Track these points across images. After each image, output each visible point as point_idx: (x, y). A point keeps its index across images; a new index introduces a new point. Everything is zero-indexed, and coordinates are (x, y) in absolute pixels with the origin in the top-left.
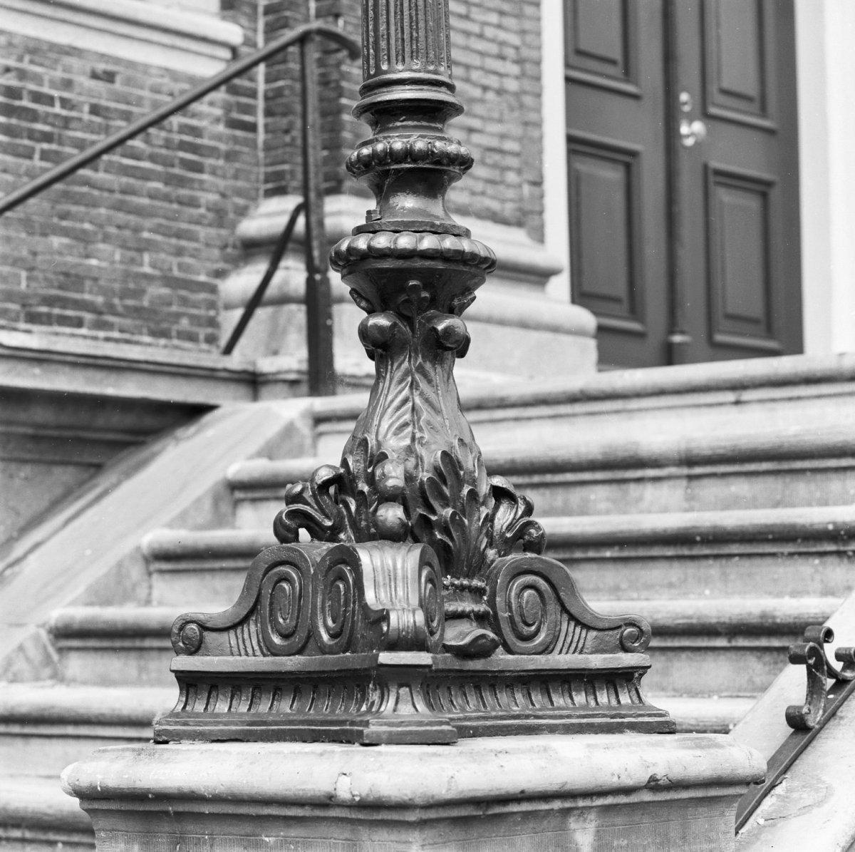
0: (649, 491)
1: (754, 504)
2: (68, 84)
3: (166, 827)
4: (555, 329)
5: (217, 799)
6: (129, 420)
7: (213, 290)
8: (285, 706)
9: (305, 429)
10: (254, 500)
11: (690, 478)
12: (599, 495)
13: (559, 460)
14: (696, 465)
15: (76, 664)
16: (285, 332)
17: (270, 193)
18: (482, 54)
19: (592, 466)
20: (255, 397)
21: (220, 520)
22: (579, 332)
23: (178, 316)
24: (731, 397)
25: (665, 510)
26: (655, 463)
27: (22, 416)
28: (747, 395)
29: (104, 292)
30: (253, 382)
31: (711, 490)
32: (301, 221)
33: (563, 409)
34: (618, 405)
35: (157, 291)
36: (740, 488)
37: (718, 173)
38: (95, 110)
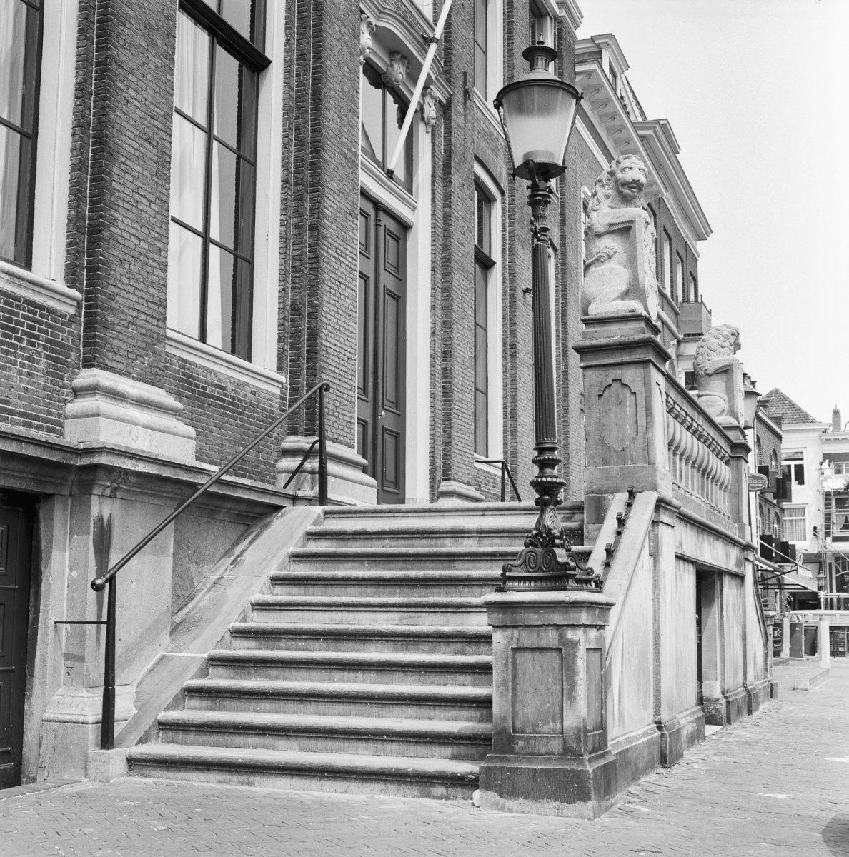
0: (466, 541)
1: (501, 545)
2: (245, 395)
3: (511, 610)
4: (367, 485)
5: (530, 603)
6: (259, 510)
7: (275, 467)
8: (544, 584)
9: (322, 515)
10: (314, 539)
11: (480, 537)
12: (448, 541)
13: (421, 528)
14: (482, 534)
15: (278, 589)
16: (303, 483)
17: (290, 434)
18: (347, 389)
19: (447, 532)
20: (294, 504)
21: (304, 546)
22: (373, 486)
23: (267, 475)
24: (481, 513)
25: (471, 546)
26: (469, 532)
27: (238, 507)
28: (486, 513)
29: (251, 466)
30: (295, 499)
31: (487, 541)
32: (317, 445)
33: (420, 514)
34: (441, 514)
35: (263, 466)
36: (497, 541)
37: (387, 429)
38: (251, 404)
